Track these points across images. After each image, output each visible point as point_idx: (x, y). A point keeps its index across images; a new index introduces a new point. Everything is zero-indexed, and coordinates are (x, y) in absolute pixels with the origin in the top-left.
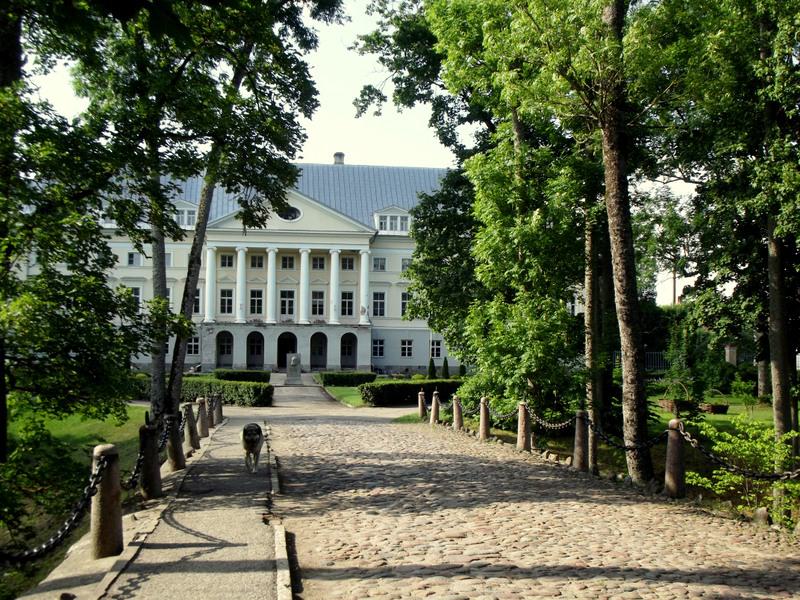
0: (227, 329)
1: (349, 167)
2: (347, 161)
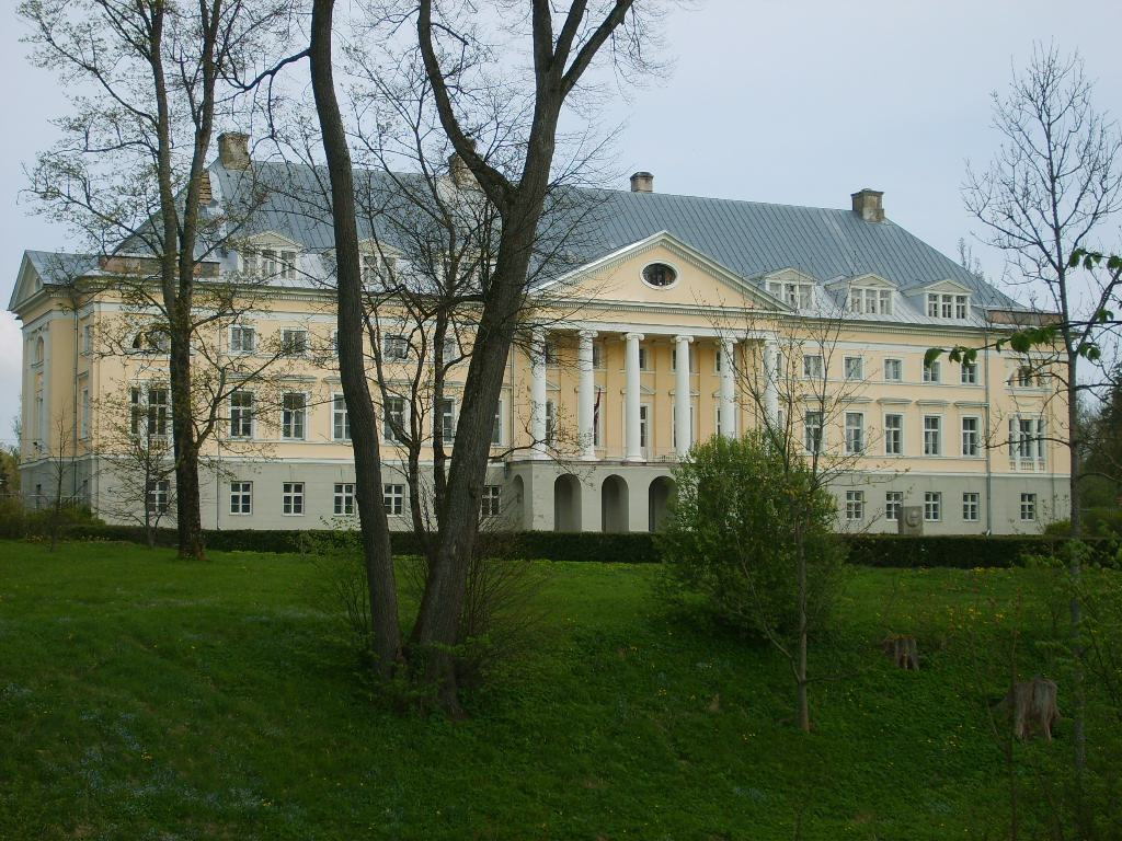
0: (574, 470)
1: (659, 197)
2: (658, 187)
